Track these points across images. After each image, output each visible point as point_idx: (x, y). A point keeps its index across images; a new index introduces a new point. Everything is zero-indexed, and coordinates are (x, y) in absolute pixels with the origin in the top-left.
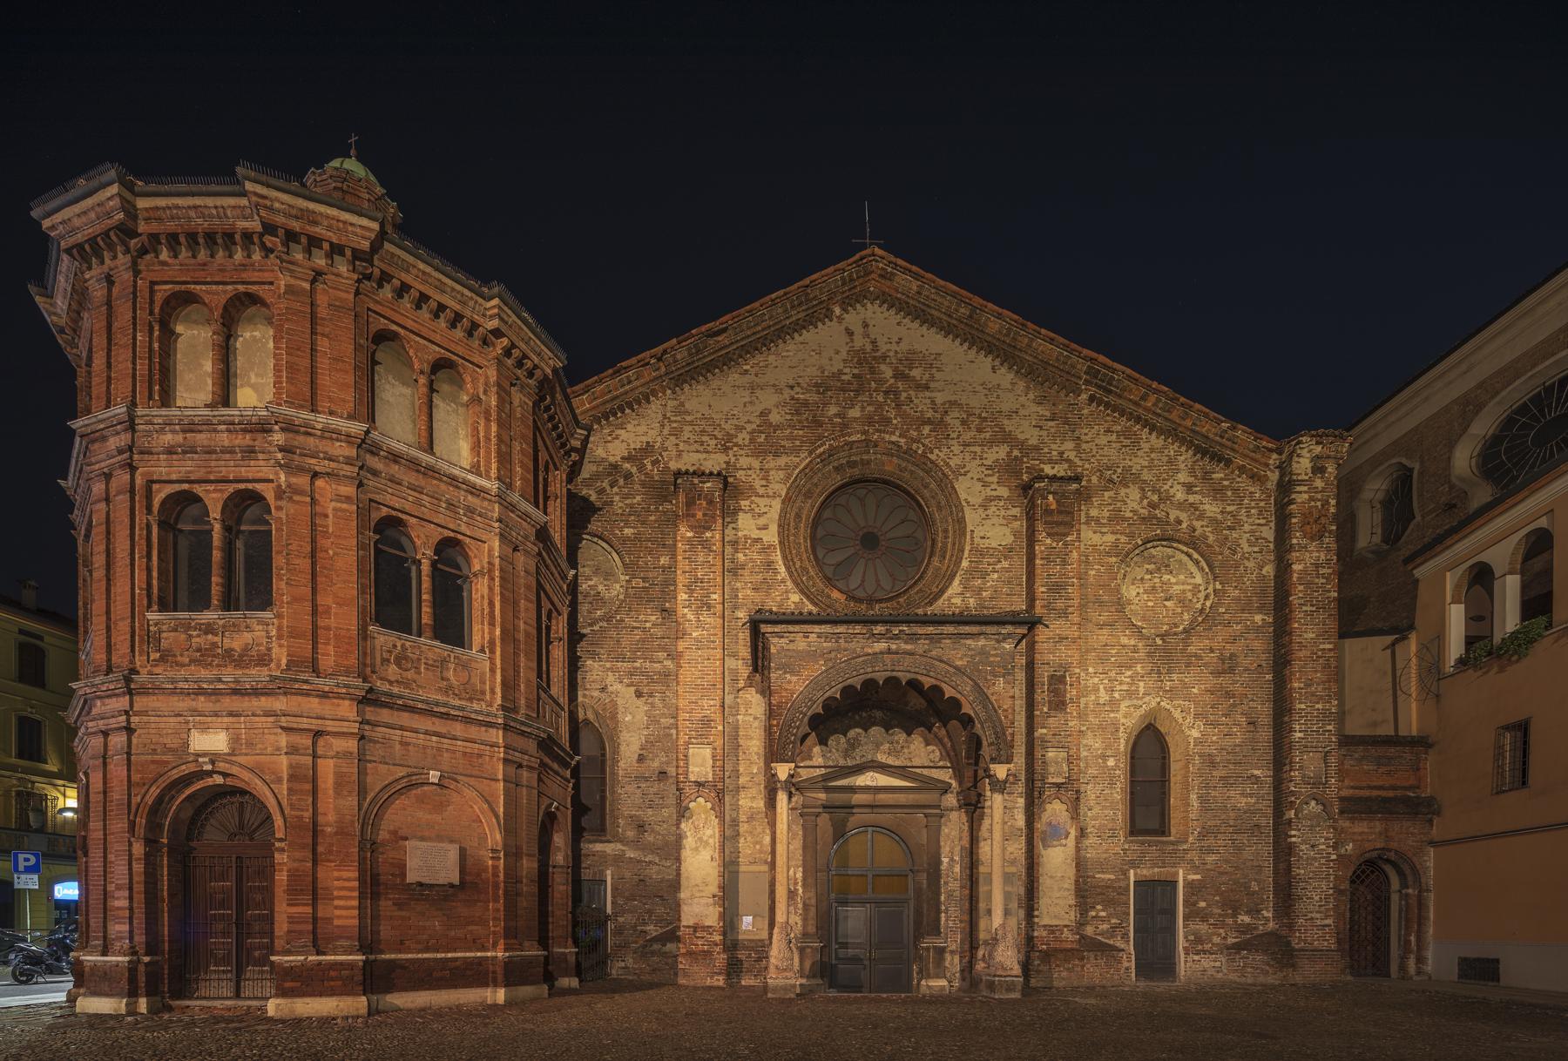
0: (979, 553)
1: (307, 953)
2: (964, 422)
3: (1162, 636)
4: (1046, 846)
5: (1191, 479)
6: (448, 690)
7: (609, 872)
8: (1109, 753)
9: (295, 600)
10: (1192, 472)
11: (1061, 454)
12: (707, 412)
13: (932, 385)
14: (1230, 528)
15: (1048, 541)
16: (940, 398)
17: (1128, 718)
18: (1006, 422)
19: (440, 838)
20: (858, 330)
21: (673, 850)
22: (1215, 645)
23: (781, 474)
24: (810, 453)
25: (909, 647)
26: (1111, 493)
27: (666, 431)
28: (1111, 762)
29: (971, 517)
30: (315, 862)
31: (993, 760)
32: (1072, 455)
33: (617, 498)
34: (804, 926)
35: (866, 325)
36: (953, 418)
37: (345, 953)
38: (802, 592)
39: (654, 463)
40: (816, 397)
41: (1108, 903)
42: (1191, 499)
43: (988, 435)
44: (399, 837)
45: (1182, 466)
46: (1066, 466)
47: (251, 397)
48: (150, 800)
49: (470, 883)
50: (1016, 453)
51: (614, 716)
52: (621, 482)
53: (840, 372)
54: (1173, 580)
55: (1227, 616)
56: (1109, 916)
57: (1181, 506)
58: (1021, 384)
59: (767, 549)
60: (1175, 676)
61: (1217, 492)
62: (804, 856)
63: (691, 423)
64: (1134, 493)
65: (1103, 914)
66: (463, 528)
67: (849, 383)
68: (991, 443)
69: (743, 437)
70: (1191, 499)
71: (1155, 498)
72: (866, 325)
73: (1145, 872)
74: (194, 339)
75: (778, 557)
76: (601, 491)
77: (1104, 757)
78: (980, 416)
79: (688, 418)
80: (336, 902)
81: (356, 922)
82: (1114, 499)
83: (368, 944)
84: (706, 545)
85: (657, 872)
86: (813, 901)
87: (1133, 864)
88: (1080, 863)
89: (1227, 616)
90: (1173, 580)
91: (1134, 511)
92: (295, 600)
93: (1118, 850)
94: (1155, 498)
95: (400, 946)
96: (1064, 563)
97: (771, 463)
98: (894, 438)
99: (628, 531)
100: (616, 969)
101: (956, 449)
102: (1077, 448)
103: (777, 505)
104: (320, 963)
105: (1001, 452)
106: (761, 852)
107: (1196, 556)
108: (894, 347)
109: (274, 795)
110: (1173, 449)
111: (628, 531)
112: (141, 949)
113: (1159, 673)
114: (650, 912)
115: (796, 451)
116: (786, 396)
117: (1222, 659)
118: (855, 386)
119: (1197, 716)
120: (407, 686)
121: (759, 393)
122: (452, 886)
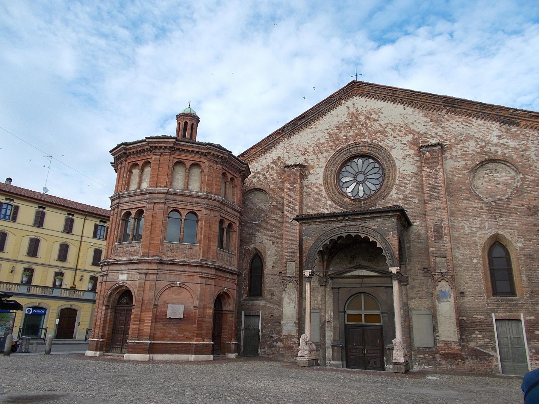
0: (403, 177)
1: (135, 340)
2: (393, 130)
3: (495, 202)
4: (439, 302)
5: (500, 134)
6: (186, 256)
7: (260, 312)
8: (473, 256)
9: (146, 237)
10: (500, 130)
11: (436, 134)
12: (298, 143)
13: (379, 119)
14: (523, 150)
15: (428, 170)
16: (383, 123)
17: (482, 237)
18: (411, 126)
19: (178, 303)
20: (351, 106)
21: (280, 303)
22: (524, 203)
23: (324, 159)
24: (335, 151)
25: (353, 223)
26: (462, 145)
27: (285, 152)
28: (475, 261)
29: (398, 163)
30: (141, 312)
31: (391, 266)
32: (441, 133)
33: (268, 176)
34: (334, 337)
35: (354, 104)
36: (389, 129)
37: (145, 340)
38: (332, 200)
39: (280, 163)
40: (336, 131)
41: (481, 331)
42: (501, 141)
43: (403, 133)
44: (166, 303)
45: (495, 129)
46: (439, 138)
47: (145, 186)
48: (108, 294)
49: (187, 318)
50: (416, 137)
51: (265, 252)
52: (270, 171)
53: (345, 121)
54: (500, 176)
55: (528, 189)
56: (484, 337)
57: (496, 145)
58: (417, 111)
59: (318, 187)
60: (504, 219)
61: (515, 137)
62: (333, 306)
63: (293, 148)
64: (472, 143)
65: (480, 336)
66: (195, 208)
67: (348, 124)
68: (405, 135)
69: (310, 149)
70: (501, 141)
71: (483, 144)
72: (354, 104)
73: (501, 314)
74: (136, 172)
75: (323, 189)
76: (264, 175)
77: (471, 258)
78: (400, 126)
79: (292, 146)
80: (145, 324)
81: (149, 330)
82: (463, 147)
83: (152, 337)
84: (294, 189)
85: (276, 313)
86: (338, 326)
87: (493, 311)
88: (459, 311)
89: (528, 189)
90: (500, 176)
91: (473, 151)
92: (146, 237)
93: (484, 303)
94: (483, 144)
95: (163, 338)
96: (436, 178)
97: (320, 156)
98: (365, 140)
99: (272, 186)
100: (261, 351)
101: (391, 139)
102: (443, 130)
103: (323, 170)
104: (138, 343)
105: (410, 137)
106: (317, 304)
107: (508, 164)
108: (365, 109)
109: (134, 291)
110: (488, 124)
111: (272, 186)
112: (100, 337)
113: (495, 218)
114: (275, 329)
115: (329, 150)
116: (326, 133)
117: (529, 208)
118: (351, 125)
119: (519, 236)
120: (173, 257)
121: (316, 134)
122: (180, 319)
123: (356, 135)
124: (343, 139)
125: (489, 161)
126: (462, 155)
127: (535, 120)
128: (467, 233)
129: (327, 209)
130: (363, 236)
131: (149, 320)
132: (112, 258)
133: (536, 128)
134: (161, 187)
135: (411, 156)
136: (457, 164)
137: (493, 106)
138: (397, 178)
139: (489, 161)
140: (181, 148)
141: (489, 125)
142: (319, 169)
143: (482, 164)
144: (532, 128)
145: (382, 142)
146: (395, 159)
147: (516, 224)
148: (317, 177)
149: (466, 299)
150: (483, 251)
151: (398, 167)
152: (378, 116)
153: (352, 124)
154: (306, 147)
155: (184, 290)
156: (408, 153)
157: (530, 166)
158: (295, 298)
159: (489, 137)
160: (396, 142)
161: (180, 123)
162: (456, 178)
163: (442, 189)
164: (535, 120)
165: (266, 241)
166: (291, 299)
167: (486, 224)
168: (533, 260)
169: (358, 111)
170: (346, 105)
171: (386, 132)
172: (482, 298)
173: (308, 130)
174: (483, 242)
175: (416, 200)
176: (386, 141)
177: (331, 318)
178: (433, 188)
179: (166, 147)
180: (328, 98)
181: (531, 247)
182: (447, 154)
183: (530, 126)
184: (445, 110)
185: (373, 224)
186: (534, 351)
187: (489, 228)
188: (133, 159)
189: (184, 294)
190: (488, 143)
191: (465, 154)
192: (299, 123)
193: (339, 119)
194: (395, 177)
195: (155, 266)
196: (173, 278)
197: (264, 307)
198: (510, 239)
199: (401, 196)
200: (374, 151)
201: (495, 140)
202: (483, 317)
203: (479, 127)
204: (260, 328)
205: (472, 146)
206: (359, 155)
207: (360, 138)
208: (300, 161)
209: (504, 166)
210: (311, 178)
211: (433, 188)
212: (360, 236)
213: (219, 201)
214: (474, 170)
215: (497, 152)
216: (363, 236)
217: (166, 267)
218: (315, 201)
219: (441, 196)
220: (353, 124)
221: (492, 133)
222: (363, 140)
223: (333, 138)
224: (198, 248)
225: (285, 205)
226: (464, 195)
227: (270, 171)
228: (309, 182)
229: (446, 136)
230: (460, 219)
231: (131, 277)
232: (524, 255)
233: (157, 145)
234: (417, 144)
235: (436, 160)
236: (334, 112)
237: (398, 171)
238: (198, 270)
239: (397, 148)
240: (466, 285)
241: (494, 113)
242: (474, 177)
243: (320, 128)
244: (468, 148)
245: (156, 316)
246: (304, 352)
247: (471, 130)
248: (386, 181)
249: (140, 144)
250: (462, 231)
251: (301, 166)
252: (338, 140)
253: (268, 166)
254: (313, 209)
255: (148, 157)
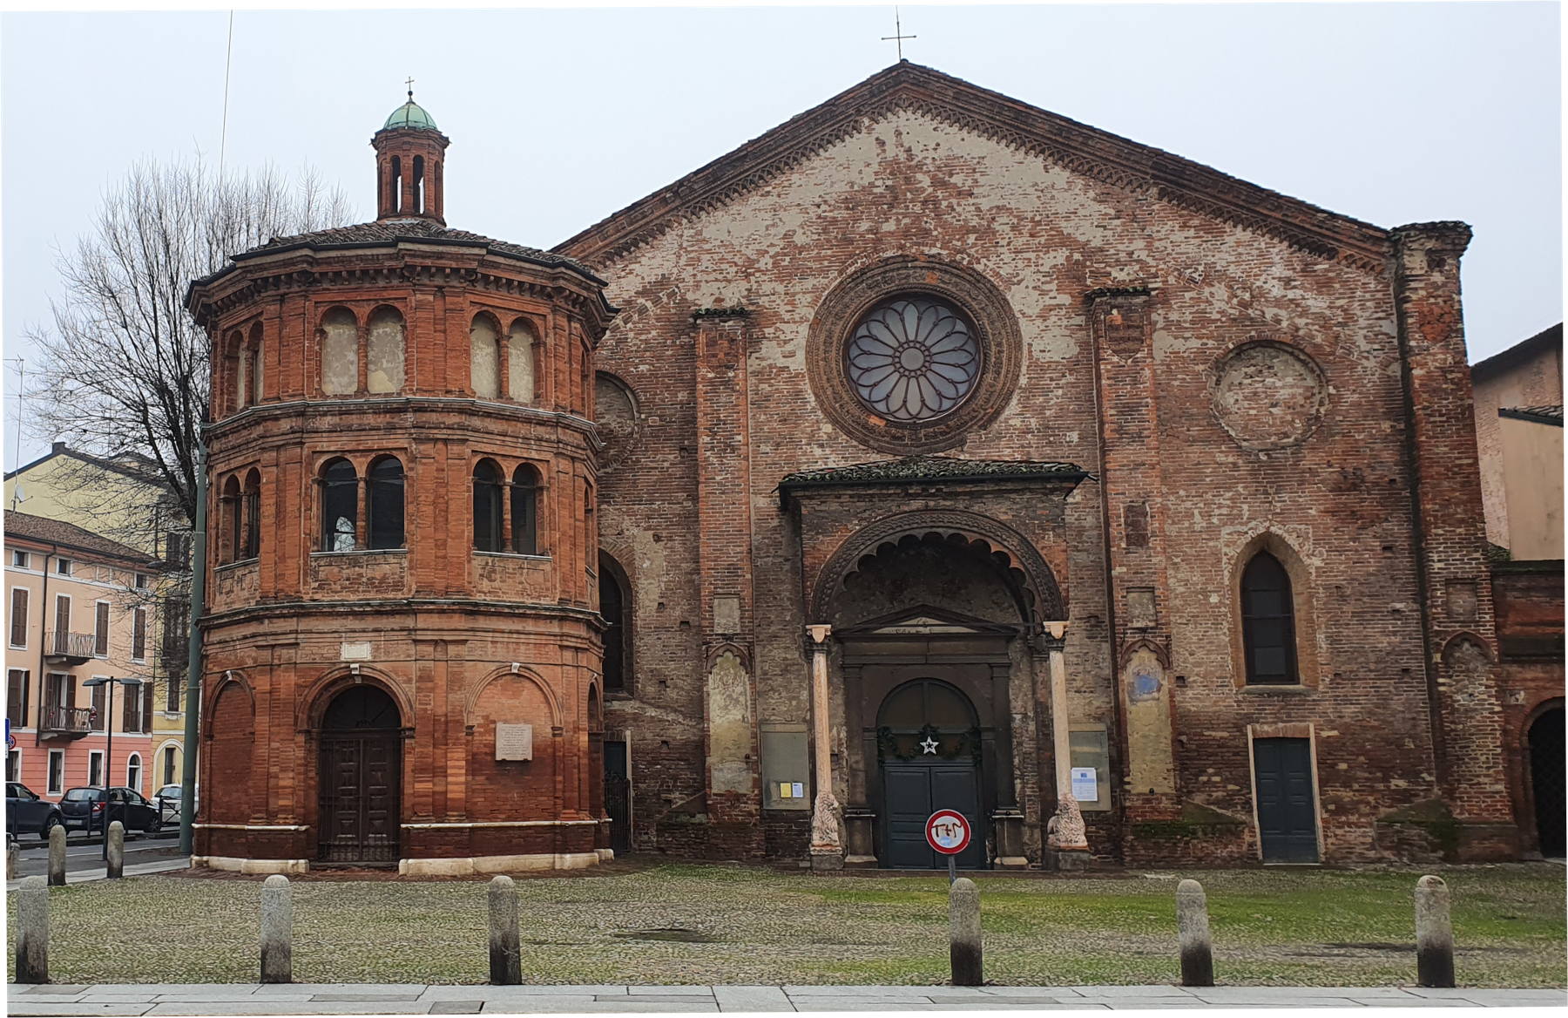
0: (1039, 368)
2: (1014, 228)
3: (1267, 451)
7: (628, 733)
10: (1289, 264)
11: (1131, 254)
12: (725, 237)
15: (1115, 359)
17: (1231, 546)
18: (1063, 224)
19: (517, 720)
23: (809, 298)
24: (841, 273)
26: (1193, 294)
27: (683, 262)
28: (1214, 599)
29: (1027, 330)
32: (1143, 255)
33: (631, 335)
34: (852, 793)
35: (898, 134)
36: (1002, 225)
38: (834, 422)
39: (669, 296)
40: (845, 213)
42: (1291, 294)
43: (1043, 240)
44: (490, 725)
45: (1277, 259)
46: (1137, 267)
49: (547, 758)
50: (1077, 256)
51: (631, 563)
52: (636, 317)
53: (872, 185)
54: (1279, 384)
57: (1278, 303)
58: (1080, 182)
60: (1286, 497)
61: (1323, 285)
63: (709, 252)
64: (1220, 291)
65: (1217, 779)
66: (534, 455)
67: (882, 196)
68: (1048, 247)
69: (766, 262)
71: (1247, 296)
72: (898, 134)
77: (1205, 593)
79: (706, 247)
82: (1198, 300)
84: (728, 384)
86: (861, 766)
88: (1180, 721)
90: (1279, 384)
91: (1222, 312)
94: (1247, 296)
96: (1135, 382)
98: (934, 251)
101: (1007, 257)
102: (1149, 247)
103: (804, 330)
104: (439, 829)
105: (1060, 257)
106: (798, 708)
108: (931, 154)
110: (1262, 242)
113: (1266, 493)
115: (823, 271)
119: (1317, 542)
121: (782, 214)
122: (525, 761)
123: (906, 234)
124: (865, 241)
125: (1257, 346)
126: (1193, 322)
127: (1375, 249)
128: (1197, 527)
129: (822, 446)
130: (971, 538)
131: (460, 768)
132: (306, 597)
133: (1372, 269)
134: (448, 392)
135: (1063, 312)
136: (1179, 345)
137: (1278, 196)
138: (1024, 369)
139: (1257, 346)
140: (493, 273)
141: (1263, 245)
142: (794, 327)
143: (1241, 351)
144: (1363, 266)
145: (984, 261)
146: (1018, 315)
147: (1313, 512)
148: (788, 348)
149: (1190, 693)
150: (1232, 575)
151: (1026, 340)
152: (970, 182)
153: (895, 198)
154: (750, 252)
155: (528, 684)
156: (1054, 302)
157: (1353, 367)
158: (744, 693)
159: (1262, 279)
160: (1021, 265)
161: (396, 161)
162: (1176, 383)
163: (1149, 414)
164: (1375, 249)
165: (635, 531)
166: (730, 696)
167: (1245, 507)
168: (1343, 598)
169: (910, 157)
170: (875, 136)
171: (994, 233)
172: (1226, 690)
173: (754, 200)
174: (1233, 552)
175: (1074, 436)
176: (994, 258)
177: (840, 745)
178: (1128, 410)
179: (456, 271)
180: (823, 106)
181: (1342, 568)
182: (1157, 316)
183: (1360, 263)
184: (1154, 191)
185: (1002, 510)
186: (1332, 807)
187: (1250, 519)
188: (333, 294)
189: (528, 692)
190: (1259, 295)
191: (1201, 320)
192: (729, 174)
193: (854, 176)
194: (1018, 366)
195: (459, 622)
196: (501, 652)
197: (636, 717)
198: (1297, 548)
199: (1034, 423)
200: (957, 285)
201: (1277, 291)
202: (1225, 734)
203: (1240, 250)
204: (629, 776)
205: (1219, 299)
206: (914, 292)
207: (918, 244)
208: (733, 296)
209: (1291, 360)
210: (771, 352)
211: (1128, 410)
212: (964, 538)
213: (583, 433)
214: (1220, 366)
215: (1279, 322)
216: (971, 538)
217: (482, 622)
218: (784, 421)
219: (1146, 433)
220: (896, 198)
221: (1271, 267)
222: (926, 250)
223: (834, 234)
224: (547, 567)
225: (702, 429)
226: (1194, 431)
227: (636, 317)
228: (764, 363)
229: (1153, 263)
230: (1182, 493)
231: (387, 653)
232: (1326, 588)
233: (428, 262)
234: (1080, 279)
235: (1136, 334)
236: (837, 151)
237: (1025, 351)
238: (555, 628)
239: (1023, 284)
240: (1191, 659)
241: (1279, 216)
242: (1218, 383)
243: (794, 196)
244: (1211, 304)
245: (474, 755)
246: (826, 831)
247: (1218, 256)
248: (989, 378)
249: (368, 252)
250: (1187, 524)
251: (739, 313)
252: (851, 241)
253: (629, 302)
254: (778, 445)
255: (394, 294)
